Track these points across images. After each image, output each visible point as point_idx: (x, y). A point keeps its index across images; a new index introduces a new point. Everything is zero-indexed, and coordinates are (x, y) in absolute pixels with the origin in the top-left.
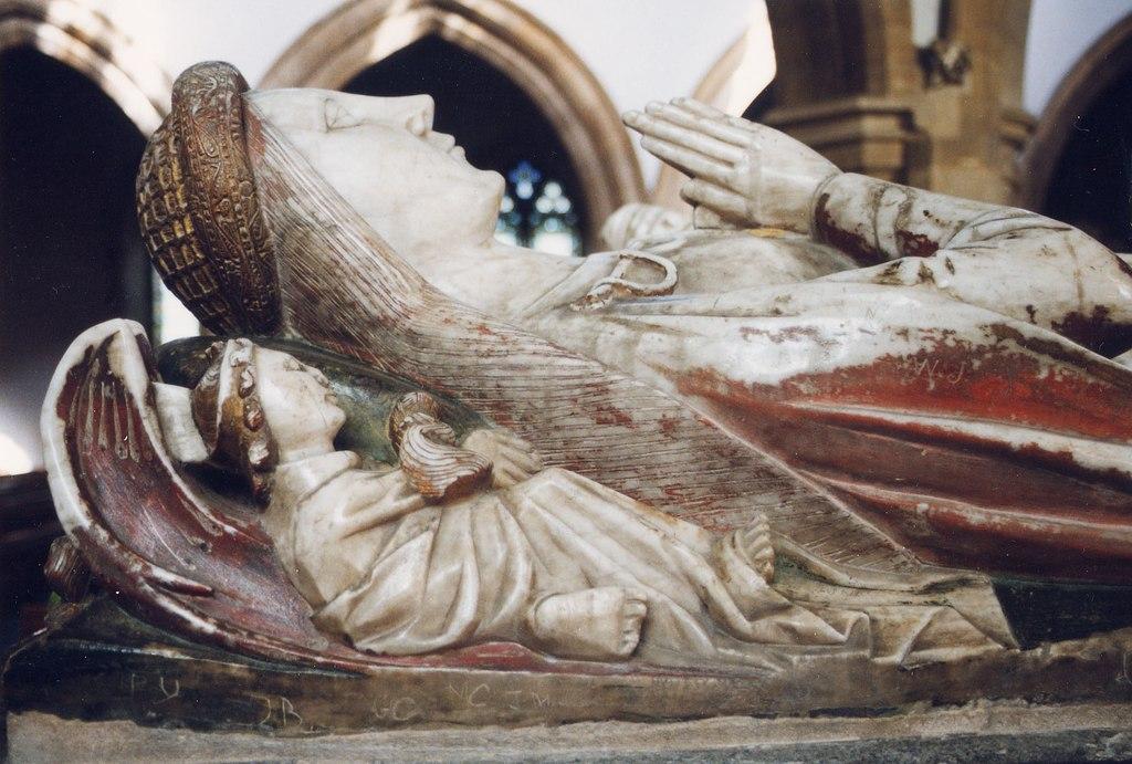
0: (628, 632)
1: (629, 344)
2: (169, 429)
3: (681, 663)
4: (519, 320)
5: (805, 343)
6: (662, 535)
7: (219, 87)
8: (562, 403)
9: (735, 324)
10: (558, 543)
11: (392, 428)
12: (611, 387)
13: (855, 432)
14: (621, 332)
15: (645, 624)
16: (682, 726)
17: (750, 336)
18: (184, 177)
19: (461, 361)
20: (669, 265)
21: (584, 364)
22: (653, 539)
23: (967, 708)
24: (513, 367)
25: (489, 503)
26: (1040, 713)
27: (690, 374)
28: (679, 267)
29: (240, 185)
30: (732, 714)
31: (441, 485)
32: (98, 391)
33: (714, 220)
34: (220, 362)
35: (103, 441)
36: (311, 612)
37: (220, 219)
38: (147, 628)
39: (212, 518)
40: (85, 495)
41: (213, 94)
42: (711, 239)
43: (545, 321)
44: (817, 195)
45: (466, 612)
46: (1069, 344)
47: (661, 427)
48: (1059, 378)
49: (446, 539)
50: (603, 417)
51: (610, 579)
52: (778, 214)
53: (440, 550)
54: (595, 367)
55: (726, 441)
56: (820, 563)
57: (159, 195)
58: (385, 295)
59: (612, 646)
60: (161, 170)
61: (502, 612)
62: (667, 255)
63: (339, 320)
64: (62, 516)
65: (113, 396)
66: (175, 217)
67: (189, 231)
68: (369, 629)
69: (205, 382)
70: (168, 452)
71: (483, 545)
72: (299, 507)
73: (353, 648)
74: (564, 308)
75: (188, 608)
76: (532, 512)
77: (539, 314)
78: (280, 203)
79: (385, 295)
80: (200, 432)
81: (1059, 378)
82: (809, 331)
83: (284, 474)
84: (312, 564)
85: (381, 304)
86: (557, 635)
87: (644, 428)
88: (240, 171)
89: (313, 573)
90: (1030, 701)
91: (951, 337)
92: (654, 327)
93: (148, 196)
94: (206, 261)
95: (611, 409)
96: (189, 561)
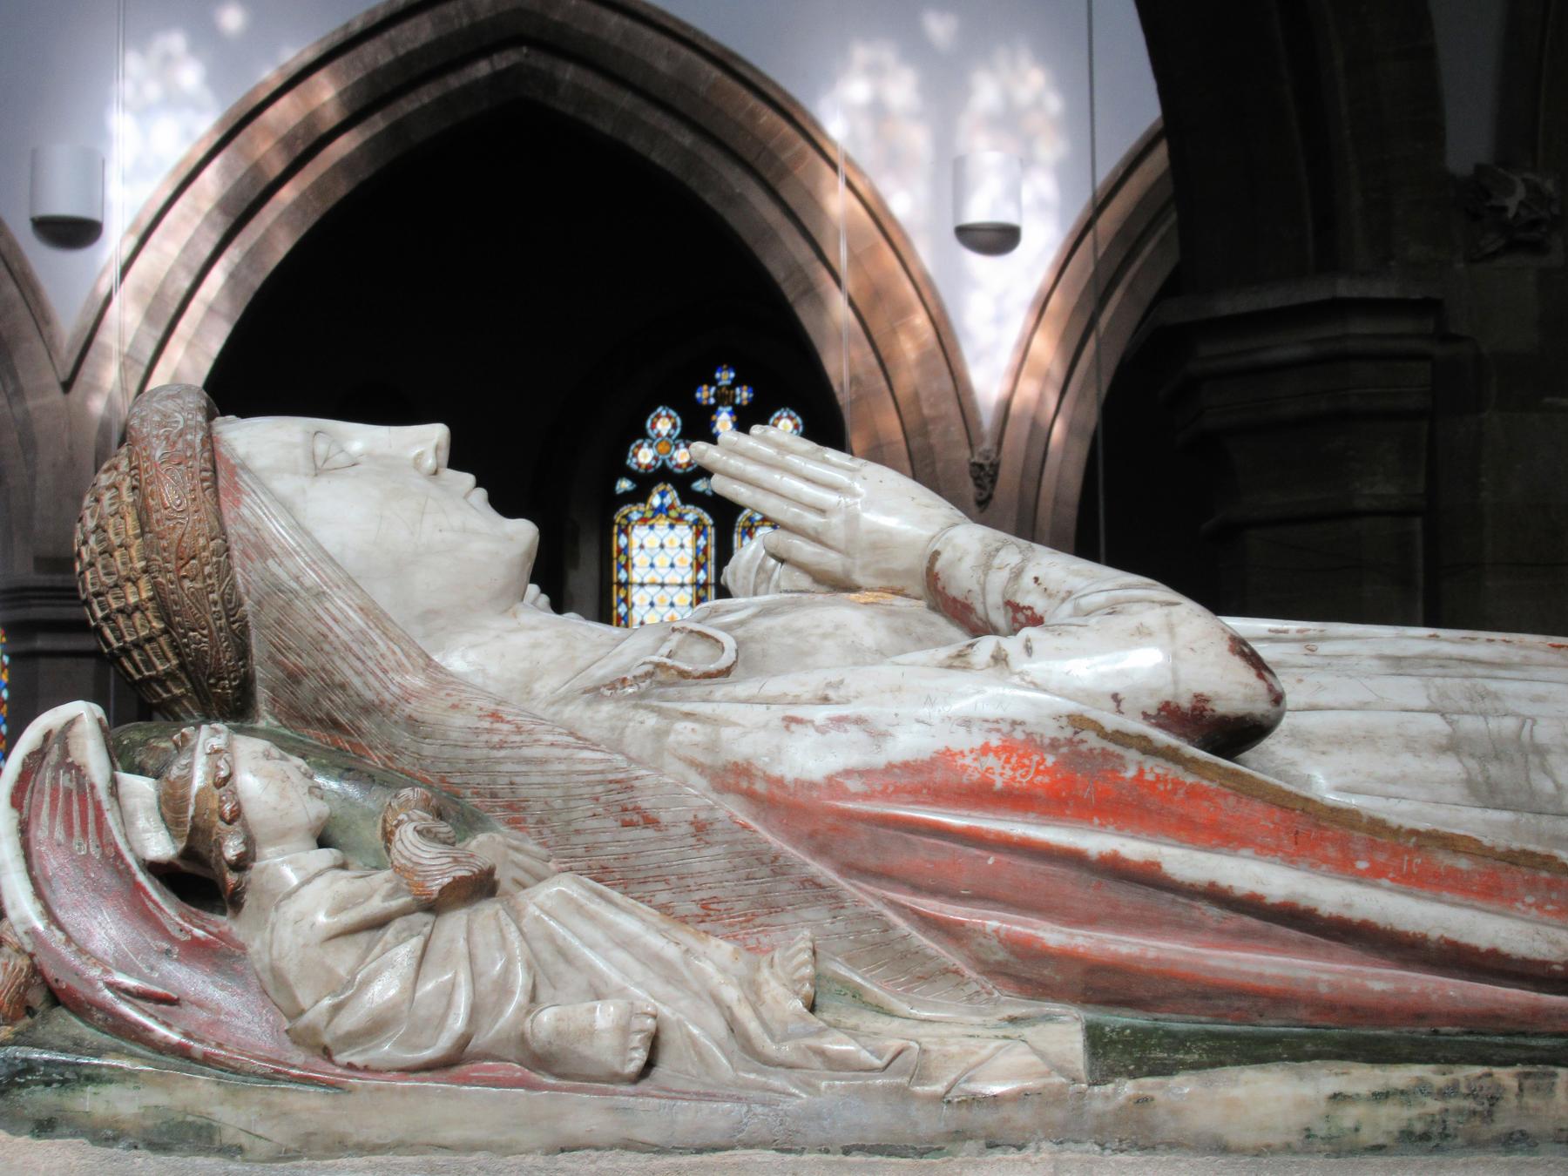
0: (635, 1049)
1: (659, 734)
2: (133, 824)
3: (694, 1088)
4: (542, 706)
5: (854, 733)
6: (684, 948)
7: (186, 426)
8: (580, 803)
9: (778, 711)
10: (564, 954)
11: (384, 829)
12: (636, 783)
13: (910, 836)
14: (652, 721)
15: (655, 1044)
16: (697, 1159)
17: (793, 727)
18: (143, 534)
19: (468, 754)
20: (729, 642)
21: (607, 756)
22: (671, 952)
23: (1028, 1152)
24: (528, 761)
25: (488, 910)
26: (1117, 1162)
27: (725, 769)
28: (741, 644)
29: (212, 544)
30: (752, 1147)
31: (435, 886)
32: (55, 779)
33: (805, 582)
34: (193, 750)
35: (59, 834)
36: (287, 1026)
37: (187, 583)
38: (106, 1039)
39: (178, 919)
40: (39, 894)
41: (181, 434)
42: (796, 605)
43: (570, 708)
44: (929, 552)
45: (457, 1023)
46: (1162, 737)
47: (692, 830)
48: (1149, 777)
49: (439, 943)
50: (627, 818)
51: (621, 992)
52: (884, 574)
53: (432, 956)
54: (619, 760)
55: (764, 846)
56: (875, 990)
57: (108, 552)
58: (381, 675)
59: (612, 1061)
60: (112, 521)
61: (497, 1027)
62: (727, 628)
63: (326, 704)
64: (12, 915)
65: (73, 786)
66: (128, 579)
67: (144, 595)
68: (353, 1039)
69: (175, 772)
70: (131, 850)
71: (480, 953)
72: (277, 909)
73: (333, 1062)
74: (595, 693)
75: (151, 1016)
76: (537, 919)
77: (566, 699)
78: (258, 565)
79: (381, 675)
80: (168, 828)
81: (1149, 777)
82: (859, 721)
83: (262, 871)
84: (291, 968)
85: (377, 685)
86: (554, 1048)
87: (673, 831)
88: (211, 529)
89: (291, 978)
90: (1102, 1146)
91: (1020, 729)
92: (688, 716)
93: (92, 551)
94: (165, 631)
95: (636, 809)
96: (152, 968)
